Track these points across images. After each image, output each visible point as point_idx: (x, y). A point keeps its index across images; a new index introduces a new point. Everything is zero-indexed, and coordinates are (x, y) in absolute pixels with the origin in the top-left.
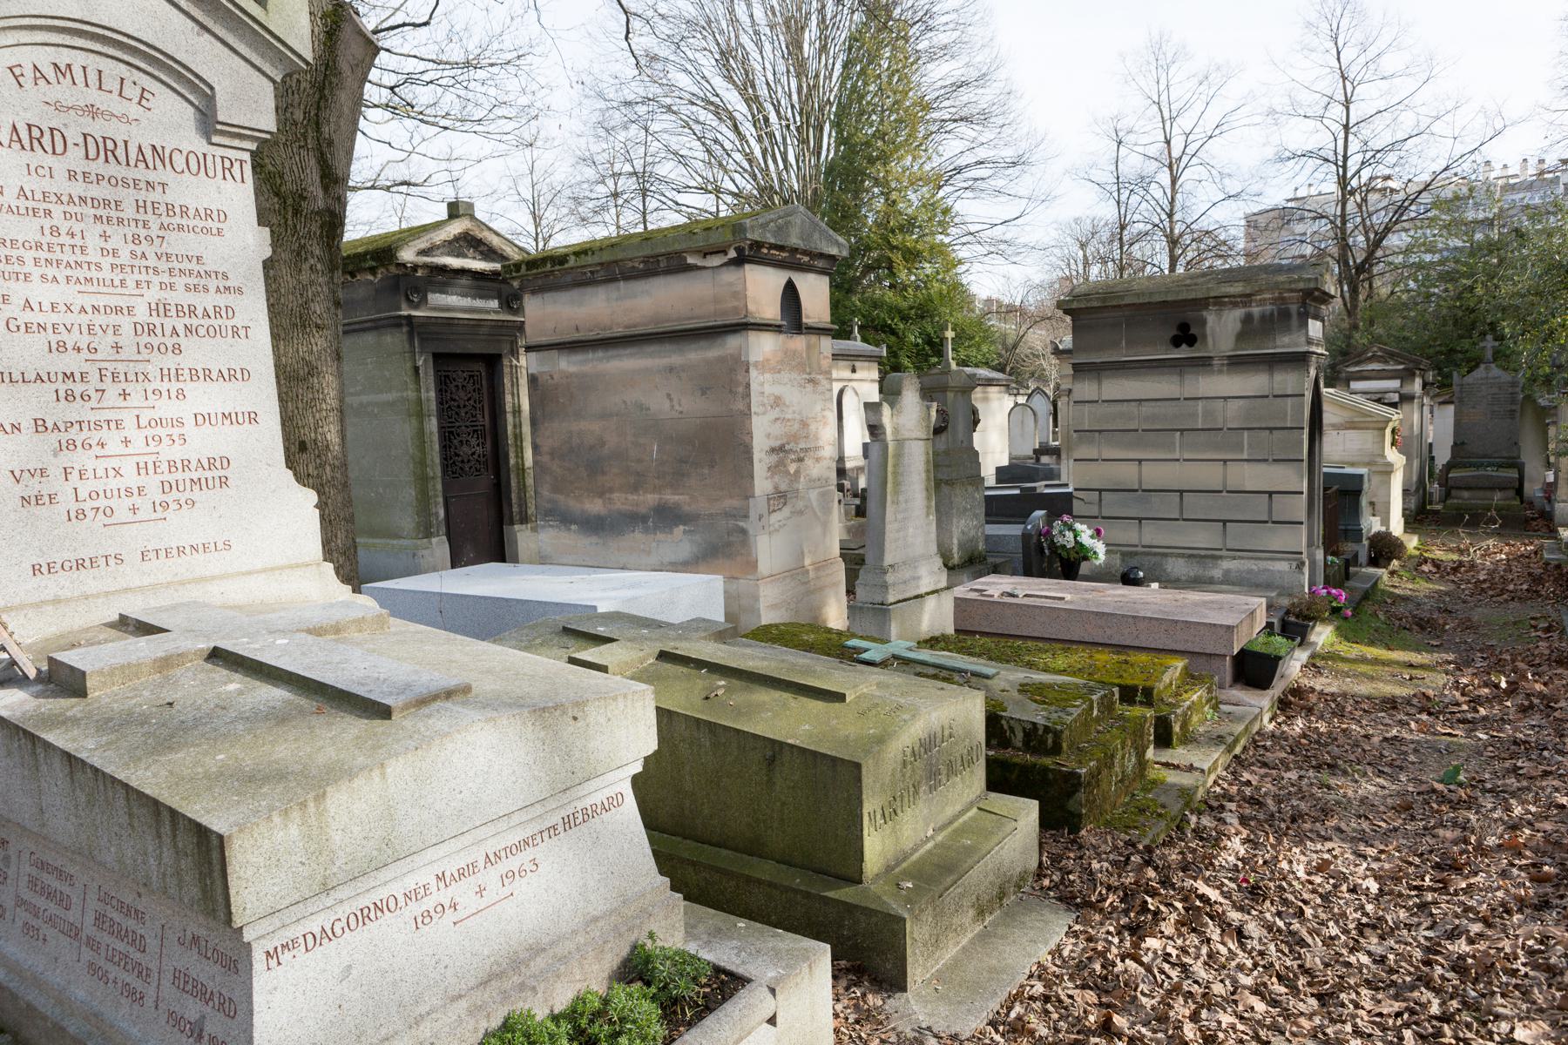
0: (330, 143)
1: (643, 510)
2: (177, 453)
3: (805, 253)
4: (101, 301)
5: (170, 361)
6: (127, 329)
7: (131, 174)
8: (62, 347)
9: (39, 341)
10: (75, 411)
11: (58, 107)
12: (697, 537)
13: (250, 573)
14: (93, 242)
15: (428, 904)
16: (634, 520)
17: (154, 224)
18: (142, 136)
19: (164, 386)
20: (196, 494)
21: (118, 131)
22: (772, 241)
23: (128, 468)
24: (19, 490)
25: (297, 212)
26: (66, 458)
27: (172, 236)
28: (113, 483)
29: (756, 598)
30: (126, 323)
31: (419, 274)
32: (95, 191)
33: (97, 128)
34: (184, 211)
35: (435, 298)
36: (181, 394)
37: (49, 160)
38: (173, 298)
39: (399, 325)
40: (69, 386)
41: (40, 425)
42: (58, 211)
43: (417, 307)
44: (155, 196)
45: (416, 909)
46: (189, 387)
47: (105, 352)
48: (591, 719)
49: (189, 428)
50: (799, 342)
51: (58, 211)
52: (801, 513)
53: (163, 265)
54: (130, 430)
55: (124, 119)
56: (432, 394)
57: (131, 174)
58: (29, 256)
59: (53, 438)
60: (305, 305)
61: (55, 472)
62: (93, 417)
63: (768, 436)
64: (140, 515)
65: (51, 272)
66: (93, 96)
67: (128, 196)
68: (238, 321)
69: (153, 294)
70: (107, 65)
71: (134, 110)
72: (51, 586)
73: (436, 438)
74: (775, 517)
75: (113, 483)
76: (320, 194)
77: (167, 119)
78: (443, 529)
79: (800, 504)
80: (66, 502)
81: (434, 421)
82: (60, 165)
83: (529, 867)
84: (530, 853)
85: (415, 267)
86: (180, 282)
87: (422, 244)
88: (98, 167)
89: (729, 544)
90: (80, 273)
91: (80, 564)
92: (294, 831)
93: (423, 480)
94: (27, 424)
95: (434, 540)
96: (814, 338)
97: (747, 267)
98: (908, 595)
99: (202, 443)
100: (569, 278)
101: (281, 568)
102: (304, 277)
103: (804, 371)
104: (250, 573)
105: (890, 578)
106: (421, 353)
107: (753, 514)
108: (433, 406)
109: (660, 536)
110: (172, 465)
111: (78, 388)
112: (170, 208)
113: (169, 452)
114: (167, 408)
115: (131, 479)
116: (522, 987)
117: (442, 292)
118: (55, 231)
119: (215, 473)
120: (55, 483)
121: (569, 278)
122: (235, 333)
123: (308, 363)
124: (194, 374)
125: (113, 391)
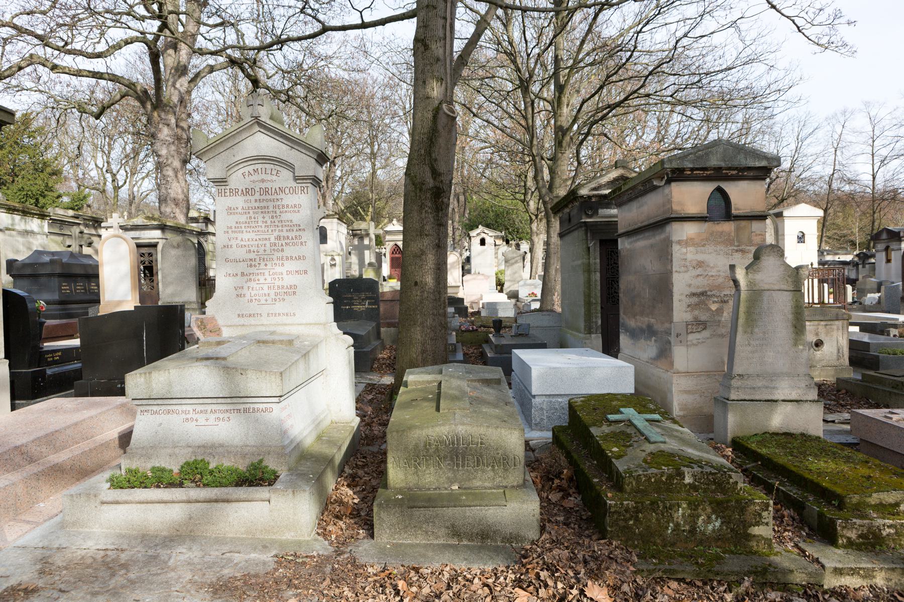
0: (436, 160)
1: (644, 327)
2: (280, 283)
3: (697, 169)
4: (261, 237)
5: (280, 254)
6: (268, 245)
7: (273, 197)
8: (250, 251)
9: (244, 249)
10: (252, 270)
11: (254, 182)
14: (260, 219)
15: (189, 416)
17: (278, 212)
18: (276, 185)
19: (277, 262)
20: (285, 297)
21: (268, 185)
22: (691, 166)
23: (266, 287)
24: (236, 292)
25: (421, 190)
26: (249, 284)
27: (283, 215)
28: (261, 292)
30: (268, 243)
31: (593, 200)
32: (262, 204)
33: (263, 186)
34: (288, 206)
35: (603, 212)
36: (283, 264)
37: (251, 198)
38: (282, 234)
39: (581, 227)
40: (251, 263)
41: (243, 274)
42: (251, 212)
43: (591, 217)
44: (278, 203)
45: (184, 416)
46: (285, 262)
47: (261, 252)
48: (249, 376)
49: (285, 276)
50: (728, 227)
51: (251, 212)
53: (280, 224)
54: (267, 276)
55: (272, 181)
56: (598, 261)
57: (273, 197)
58: (243, 226)
59: (246, 278)
60: (422, 227)
61: (245, 288)
62: (257, 272)
63: (690, 285)
64: (268, 302)
65: (248, 230)
66: (264, 176)
67: (271, 204)
68: (303, 240)
69: (276, 234)
70: (267, 166)
71: (274, 178)
72: (242, 321)
73: (599, 283)
74: (691, 337)
75: (261, 292)
76: (432, 181)
77: (284, 178)
80: (248, 297)
81: (598, 274)
82: (253, 198)
83: (226, 418)
84: (228, 415)
85: (590, 197)
86: (285, 229)
87: (593, 185)
88: (264, 197)
90: (256, 229)
91: (250, 315)
92: (142, 379)
93: (588, 304)
94: (239, 274)
95: (593, 336)
96: (743, 223)
97: (673, 184)
98: (757, 398)
99: (289, 280)
100: (625, 198)
102: (423, 215)
103: (732, 244)
105: (734, 383)
106: (592, 240)
108: (598, 267)
110: (278, 287)
111: (253, 263)
112: (283, 206)
113: (277, 283)
114: (278, 269)
115: (266, 291)
116: (210, 454)
117: (607, 208)
118: (250, 218)
119: (292, 291)
120: (245, 291)
121: (625, 198)
122: (302, 244)
123: (421, 250)
124: (287, 259)
125: (263, 264)
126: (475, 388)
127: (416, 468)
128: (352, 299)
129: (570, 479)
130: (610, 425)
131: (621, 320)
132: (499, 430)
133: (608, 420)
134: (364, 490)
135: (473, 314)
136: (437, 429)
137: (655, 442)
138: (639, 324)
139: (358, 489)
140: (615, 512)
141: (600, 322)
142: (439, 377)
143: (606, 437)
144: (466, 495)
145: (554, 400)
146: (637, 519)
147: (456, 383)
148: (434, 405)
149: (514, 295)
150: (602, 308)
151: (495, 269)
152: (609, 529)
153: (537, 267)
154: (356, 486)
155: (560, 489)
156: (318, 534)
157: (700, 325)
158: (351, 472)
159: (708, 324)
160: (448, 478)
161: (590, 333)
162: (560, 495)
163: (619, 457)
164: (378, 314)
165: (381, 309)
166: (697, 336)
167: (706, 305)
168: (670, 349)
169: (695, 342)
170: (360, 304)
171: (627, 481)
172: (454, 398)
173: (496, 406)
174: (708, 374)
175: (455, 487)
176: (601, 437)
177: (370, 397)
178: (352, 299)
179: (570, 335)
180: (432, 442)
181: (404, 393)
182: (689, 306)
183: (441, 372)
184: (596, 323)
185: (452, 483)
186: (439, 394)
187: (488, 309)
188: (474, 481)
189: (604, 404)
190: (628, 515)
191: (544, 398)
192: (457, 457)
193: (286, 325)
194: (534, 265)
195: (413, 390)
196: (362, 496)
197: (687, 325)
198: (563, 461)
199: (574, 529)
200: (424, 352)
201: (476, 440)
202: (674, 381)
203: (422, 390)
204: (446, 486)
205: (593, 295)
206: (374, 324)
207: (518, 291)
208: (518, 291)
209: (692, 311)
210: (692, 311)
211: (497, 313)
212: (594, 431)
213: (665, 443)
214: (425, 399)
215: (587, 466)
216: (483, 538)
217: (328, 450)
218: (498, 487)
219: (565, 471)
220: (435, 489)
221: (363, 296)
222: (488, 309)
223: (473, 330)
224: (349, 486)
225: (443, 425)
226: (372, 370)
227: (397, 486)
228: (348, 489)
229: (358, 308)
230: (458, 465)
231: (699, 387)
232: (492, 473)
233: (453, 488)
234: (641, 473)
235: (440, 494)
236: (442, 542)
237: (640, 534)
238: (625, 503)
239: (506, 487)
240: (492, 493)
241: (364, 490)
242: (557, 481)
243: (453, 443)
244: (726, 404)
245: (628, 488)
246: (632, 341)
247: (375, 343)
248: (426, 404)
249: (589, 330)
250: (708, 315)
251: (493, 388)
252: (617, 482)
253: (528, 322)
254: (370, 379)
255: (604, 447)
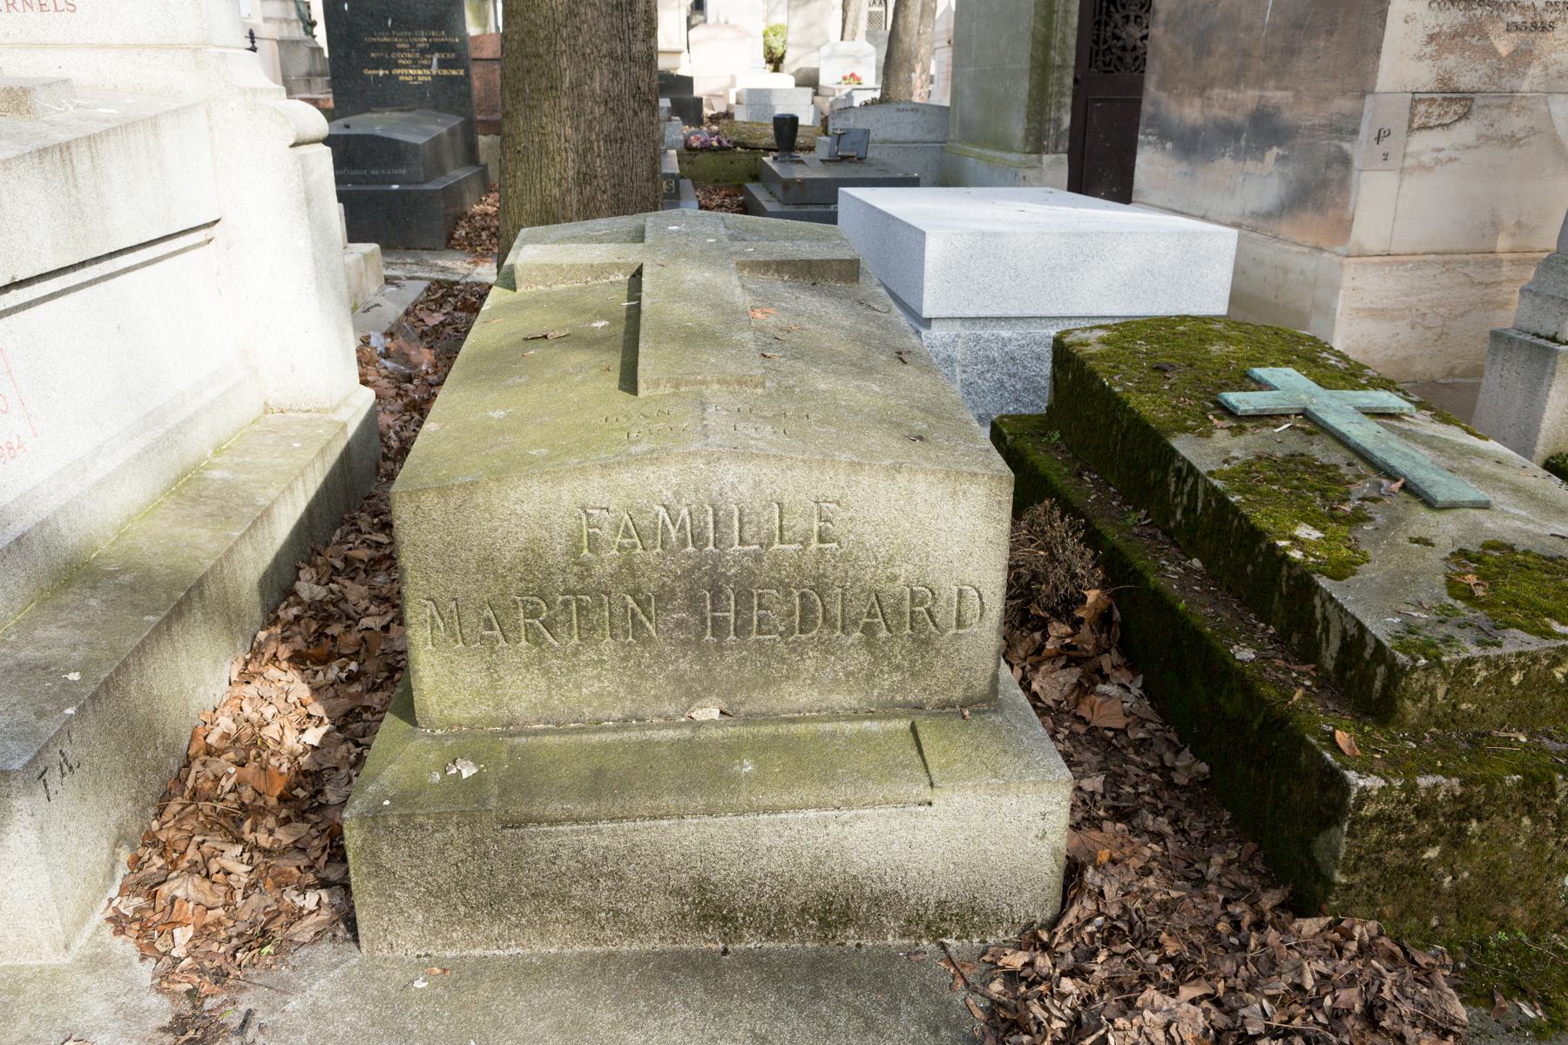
1: (1239, 118)
12: (1289, 170)
13: (103, 46)
16: (1227, 134)
29: (1335, 289)
52: (1513, 140)
74: (1422, 143)
78: (1065, 144)
79: (1516, 123)
89: (1324, 185)
93: (1042, 68)
95: (1047, 158)
101: (141, 46)
104: (103, 46)
107: (1366, 130)
109: (1250, 165)
126: (766, 299)
127: (537, 641)
128: (391, 47)
129: (1103, 619)
130: (1241, 430)
131: (1147, 108)
132: (902, 479)
133: (1227, 411)
134: (352, 678)
135: (714, 119)
136: (626, 478)
137: (1452, 506)
138: (1218, 112)
139: (333, 672)
140: (1378, 818)
141: (1067, 120)
142: (633, 254)
143: (1246, 475)
144: (760, 748)
145: (986, 333)
146: (1457, 840)
147: (694, 275)
148: (615, 360)
149: (809, 80)
150: (1076, 81)
151: (763, 27)
152: (1340, 878)
153: (857, 19)
154: (325, 660)
155: (1070, 656)
156: (119, 923)
157: (1456, 101)
158: (320, 592)
159: (1479, 100)
160: (679, 679)
161: (1039, 150)
162: (1072, 676)
163: (1340, 571)
164: (468, 94)
165: (476, 83)
166: (1438, 138)
167: (1485, 37)
168: (1344, 184)
169: (1427, 159)
170: (415, 64)
171: (1417, 681)
172: (694, 338)
173: (863, 369)
174: (1447, 258)
175: (708, 712)
176: (1227, 477)
177: (437, 318)
178: (391, 47)
179: (973, 158)
180: (605, 533)
181: (500, 309)
182: (1432, 38)
183: (639, 236)
184: (1058, 121)
185: (694, 697)
186: (634, 314)
187: (750, 105)
188: (789, 688)
189: (1166, 342)
190: (1425, 828)
191: (957, 328)
192: (717, 592)
193: (43, 45)
194: (851, 15)
195: (535, 302)
196: (344, 704)
197: (1415, 103)
198: (1081, 561)
199: (1159, 837)
200: (584, 179)
201: (800, 525)
202: (1346, 281)
203: (565, 303)
204: (670, 708)
205: (1056, 42)
206: (456, 121)
207: (817, 71)
208: (817, 71)
209: (1436, 56)
210: (1436, 56)
211: (772, 107)
212: (1184, 446)
213: (1485, 506)
214: (573, 340)
215: (1172, 574)
216: (825, 924)
217: (196, 542)
218: (887, 710)
219: (1092, 595)
220: (624, 724)
221: (422, 41)
222: (750, 105)
223: (721, 148)
224: (298, 659)
225: (653, 457)
226: (450, 243)
227: (457, 714)
228: (293, 675)
229: (409, 75)
230: (719, 626)
231: (1413, 300)
232: (863, 657)
233: (700, 715)
234: (1475, 651)
235: (644, 746)
236: (654, 944)
237: (1456, 891)
238: (1424, 782)
239: (919, 707)
240: (865, 737)
241: (352, 678)
242: (1058, 629)
243: (699, 539)
244: (1555, 353)
245: (1412, 710)
246: (1184, 167)
247: (457, 174)
248: (579, 357)
249: (1037, 144)
250: (1483, 69)
251: (831, 295)
252: (1365, 679)
253: (861, 126)
254: (444, 269)
255: (1260, 519)
